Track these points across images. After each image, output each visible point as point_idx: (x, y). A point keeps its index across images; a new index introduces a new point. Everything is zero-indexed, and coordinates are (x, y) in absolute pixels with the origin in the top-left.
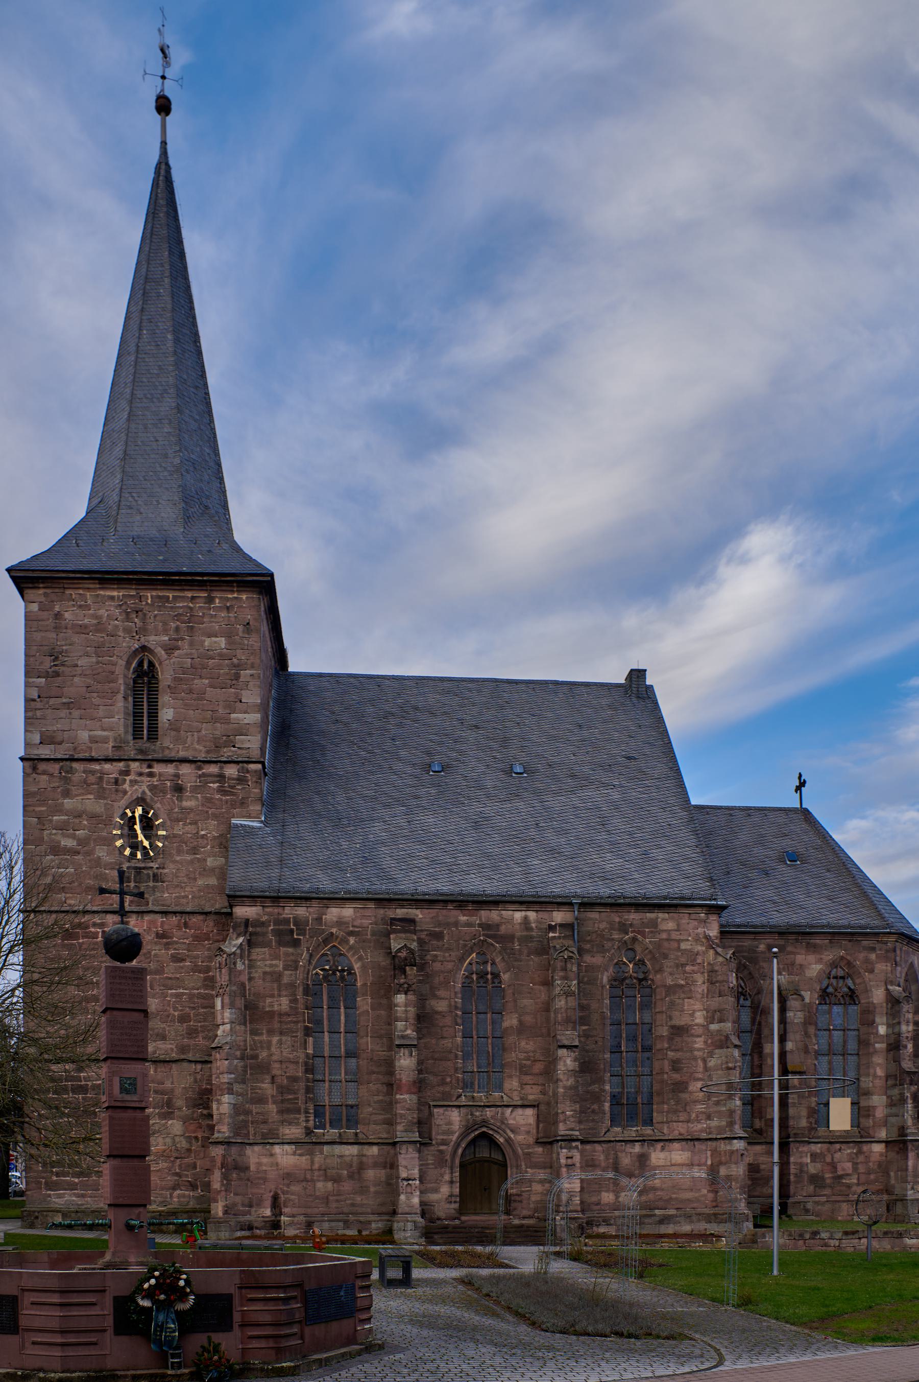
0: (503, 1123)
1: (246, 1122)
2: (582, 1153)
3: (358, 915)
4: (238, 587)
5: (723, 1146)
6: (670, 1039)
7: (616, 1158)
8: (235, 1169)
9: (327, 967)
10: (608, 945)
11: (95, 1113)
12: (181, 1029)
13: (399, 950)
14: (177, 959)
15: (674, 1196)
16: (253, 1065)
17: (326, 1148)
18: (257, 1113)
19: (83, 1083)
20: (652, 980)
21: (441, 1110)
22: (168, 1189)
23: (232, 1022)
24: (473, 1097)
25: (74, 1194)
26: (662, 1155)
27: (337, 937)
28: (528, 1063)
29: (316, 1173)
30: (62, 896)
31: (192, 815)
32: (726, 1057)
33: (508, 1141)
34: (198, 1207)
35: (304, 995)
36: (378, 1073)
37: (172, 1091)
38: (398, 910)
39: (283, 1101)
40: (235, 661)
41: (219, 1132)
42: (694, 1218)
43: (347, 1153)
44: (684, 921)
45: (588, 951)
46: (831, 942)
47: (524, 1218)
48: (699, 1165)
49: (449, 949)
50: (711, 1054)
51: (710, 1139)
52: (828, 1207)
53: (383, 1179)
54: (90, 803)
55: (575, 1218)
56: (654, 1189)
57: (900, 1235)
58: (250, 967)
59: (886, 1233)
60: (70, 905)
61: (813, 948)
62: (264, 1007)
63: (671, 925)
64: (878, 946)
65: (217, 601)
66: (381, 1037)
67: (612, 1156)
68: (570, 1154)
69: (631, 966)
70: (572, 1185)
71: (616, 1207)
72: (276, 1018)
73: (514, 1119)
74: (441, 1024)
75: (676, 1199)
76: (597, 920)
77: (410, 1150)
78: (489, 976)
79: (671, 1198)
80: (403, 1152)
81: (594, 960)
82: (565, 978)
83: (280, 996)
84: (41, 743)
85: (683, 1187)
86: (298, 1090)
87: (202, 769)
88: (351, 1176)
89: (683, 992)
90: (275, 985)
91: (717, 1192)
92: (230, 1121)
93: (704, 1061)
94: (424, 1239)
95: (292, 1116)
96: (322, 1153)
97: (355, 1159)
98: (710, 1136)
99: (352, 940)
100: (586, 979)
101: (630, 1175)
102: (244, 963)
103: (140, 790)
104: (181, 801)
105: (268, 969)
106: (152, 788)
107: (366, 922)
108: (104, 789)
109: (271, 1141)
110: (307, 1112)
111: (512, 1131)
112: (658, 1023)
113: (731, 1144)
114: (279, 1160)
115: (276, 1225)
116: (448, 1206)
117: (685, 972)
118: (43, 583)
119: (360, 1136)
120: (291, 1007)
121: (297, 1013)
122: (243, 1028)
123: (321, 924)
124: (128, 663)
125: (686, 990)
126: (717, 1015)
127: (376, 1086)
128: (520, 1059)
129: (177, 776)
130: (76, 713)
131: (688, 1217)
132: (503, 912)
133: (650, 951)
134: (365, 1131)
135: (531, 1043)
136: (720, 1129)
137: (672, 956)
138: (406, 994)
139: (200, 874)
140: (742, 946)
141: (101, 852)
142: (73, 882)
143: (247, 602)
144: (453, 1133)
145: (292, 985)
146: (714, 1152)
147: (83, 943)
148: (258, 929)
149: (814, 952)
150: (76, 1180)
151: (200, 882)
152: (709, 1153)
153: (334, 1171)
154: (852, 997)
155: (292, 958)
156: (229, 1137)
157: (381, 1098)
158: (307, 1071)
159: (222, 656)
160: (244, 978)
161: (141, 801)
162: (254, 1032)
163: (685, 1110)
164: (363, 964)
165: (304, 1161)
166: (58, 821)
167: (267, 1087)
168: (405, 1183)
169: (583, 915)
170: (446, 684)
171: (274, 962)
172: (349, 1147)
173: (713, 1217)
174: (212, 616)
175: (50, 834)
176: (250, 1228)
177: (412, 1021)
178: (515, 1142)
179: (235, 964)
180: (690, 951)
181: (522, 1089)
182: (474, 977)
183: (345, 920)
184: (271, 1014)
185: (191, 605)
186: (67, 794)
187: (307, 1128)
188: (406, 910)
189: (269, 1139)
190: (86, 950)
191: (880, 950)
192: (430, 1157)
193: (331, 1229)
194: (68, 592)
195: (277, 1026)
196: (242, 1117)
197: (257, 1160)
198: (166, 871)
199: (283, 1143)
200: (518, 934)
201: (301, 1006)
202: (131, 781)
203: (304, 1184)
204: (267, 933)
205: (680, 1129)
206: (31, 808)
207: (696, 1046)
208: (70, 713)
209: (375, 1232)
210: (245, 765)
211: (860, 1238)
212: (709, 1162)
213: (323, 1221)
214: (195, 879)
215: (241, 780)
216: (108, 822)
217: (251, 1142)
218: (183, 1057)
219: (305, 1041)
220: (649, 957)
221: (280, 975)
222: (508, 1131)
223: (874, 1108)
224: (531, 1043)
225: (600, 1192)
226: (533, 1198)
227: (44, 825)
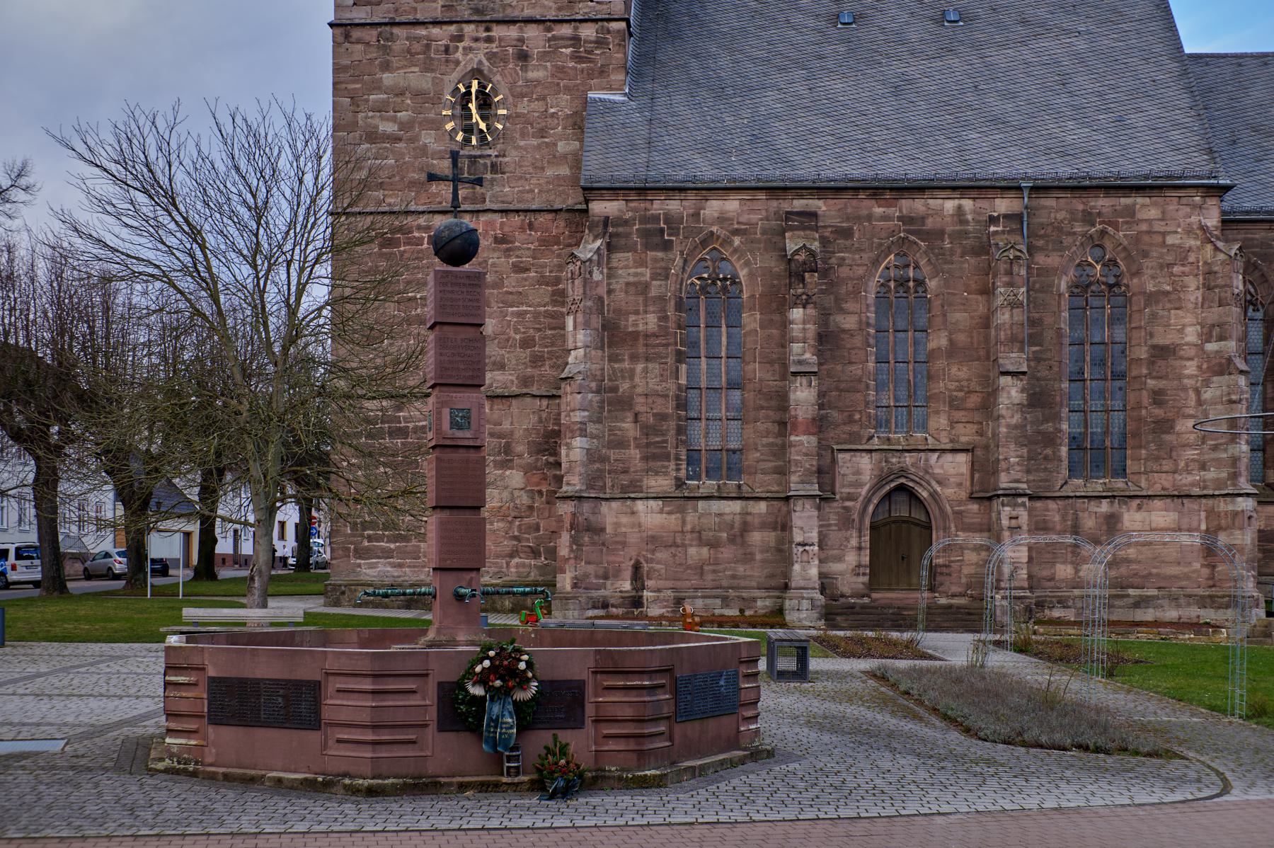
0: (927, 472)
2: (1031, 511)
3: (746, 208)
5: (1223, 506)
7: (1076, 518)
9: (706, 275)
10: (1067, 241)
14: (519, 269)
17: (701, 504)
20: (1127, 286)
21: (847, 456)
22: (503, 557)
24: (889, 439)
25: (390, 563)
27: (718, 237)
28: (961, 394)
29: (689, 536)
31: (539, 89)
32: (1228, 386)
33: (934, 495)
34: (540, 579)
36: (768, 408)
37: (512, 433)
39: (648, 445)
41: (568, 484)
42: (1182, 601)
43: (727, 510)
47: (953, 596)
49: (860, 250)
50: (1207, 383)
51: (1205, 496)
53: (772, 544)
54: (416, 78)
56: (1127, 561)
58: (609, 276)
60: (389, 205)
62: (626, 326)
63: (1153, 213)
66: (771, 362)
68: (1014, 514)
69: (1098, 268)
70: (1016, 554)
72: (641, 341)
73: (942, 467)
74: (849, 346)
76: (1054, 208)
77: (807, 506)
78: (911, 284)
79: (1150, 574)
80: (798, 508)
82: (1010, 284)
83: (646, 312)
88: (732, 540)
90: (641, 299)
91: (1214, 567)
92: (583, 470)
93: (1198, 392)
94: (823, 622)
95: (659, 464)
97: (737, 518)
98: (1205, 492)
99: (737, 241)
102: (602, 273)
103: (476, 60)
105: (631, 279)
106: (491, 56)
107: (754, 217)
109: (632, 495)
111: (939, 483)
112: (1133, 343)
113: (1233, 503)
114: (643, 520)
115: (637, 602)
116: (855, 579)
117: (1172, 274)
119: (745, 488)
121: (667, 334)
122: (600, 353)
123: (698, 221)
126: (1216, 331)
128: (950, 390)
129: (521, 40)
132: (930, 201)
133: (1125, 249)
135: (965, 369)
136: (1219, 483)
141: (428, 138)
145: (661, 299)
146: (1211, 513)
147: (404, 251)
148: (621, 229)
150: (392, 546)
151: (549, 172)
152: (1203, 514)
153: (711, 534)
155: (663, 264)
157: (771, 440)
158: (678, 407)
160: (602, 291)
161: (477, 73)
164: (749, 270)
165: (673, 520)
166: (375, 101)
167: (628, 427)
168: (801, 549)
172: (730, 503)
173: (1208, 600)
175: (367, 117)
176: (605, 606)
177: (812, 342)
178: (943, 497)
179: (591, 273)
181: (952, 428)
182: (892, 284)
184: (635, 336)
186: (386, 67)
187: (677, 479)
188: (805, 202)
189: (630, 492)
193: (706, 608)
195: (641, 350)
198: (506, 159)
201: (671, 325)
202: (464, 48)
203: (673, 550)
204: (631, 233)
206: (343, 86)
209: (762, 612)
212: (1203, 527)
213: (696, 597)
214: (543, 169)
215: (600, 43)
216: (437, 100)
217: (608, 496)
218: (525, 391)
220: (1123, 255)
221: (647, 286)
224: (965, 369)
226: (966, 571)
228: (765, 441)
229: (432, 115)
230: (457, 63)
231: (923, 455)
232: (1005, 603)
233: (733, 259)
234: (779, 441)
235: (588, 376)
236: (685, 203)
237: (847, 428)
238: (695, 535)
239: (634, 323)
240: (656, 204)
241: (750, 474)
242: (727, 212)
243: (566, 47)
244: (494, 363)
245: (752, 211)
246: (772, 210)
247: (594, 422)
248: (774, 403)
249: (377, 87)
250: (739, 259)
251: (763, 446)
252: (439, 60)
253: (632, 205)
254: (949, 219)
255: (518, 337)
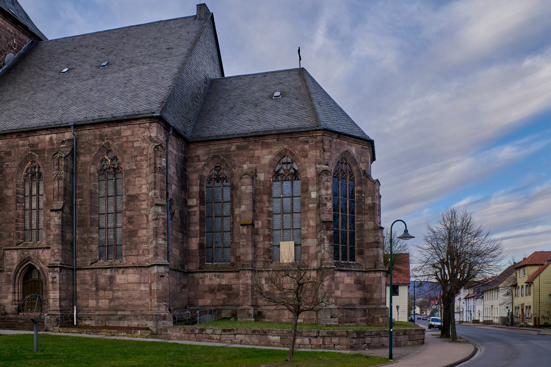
0: (38, 258)
6: (127, 203)
10: (93, 149)
15: (130, 303)
26: (123, 277)
42: (139, 317)
44: (136, 129)
45: (83, 154)
46: (277, 140)
48: (144, 283)
49: (14, 161)
52: (275, 312)
55: (54, 315)
56: (118, 298)
57: (265, 333)
59: (254, 332)
61: (267, 146)
63: (129, 132)
64: (310, 140)
67: (94, 278)
68: (54, 275)
71: (97, 309)
73: (44, 256)
75: (131, 305)
76: (88, 134)
79: (128, 304)
81: (86, 159)
85: (135, 297)
89: (135, 174)
100: (81, 171)
101: (105, 289)
111: (42, 263)
116: (12, 306)
125: (136, 172)
131: (136, 316)
132: (40, 136)
137: (129, 152)
140: (222, 148)
144: (14, 265)
149: (267, 148)
154: (295, 175)
163: (136, 248)
169: (80, 133)
170: (105, 33)
180: (140, 147)
191: (312, 142)
192: (3, 279)
200: (47, 148)
205: (133, 260)
207: (143, 207)
211: (235, 334)
222: (41, 263)
223: (308, 247)
225: (88, 299)
231: (36, 250)
232: (48, 317)
237: (9, 239)
254: (47, 144)
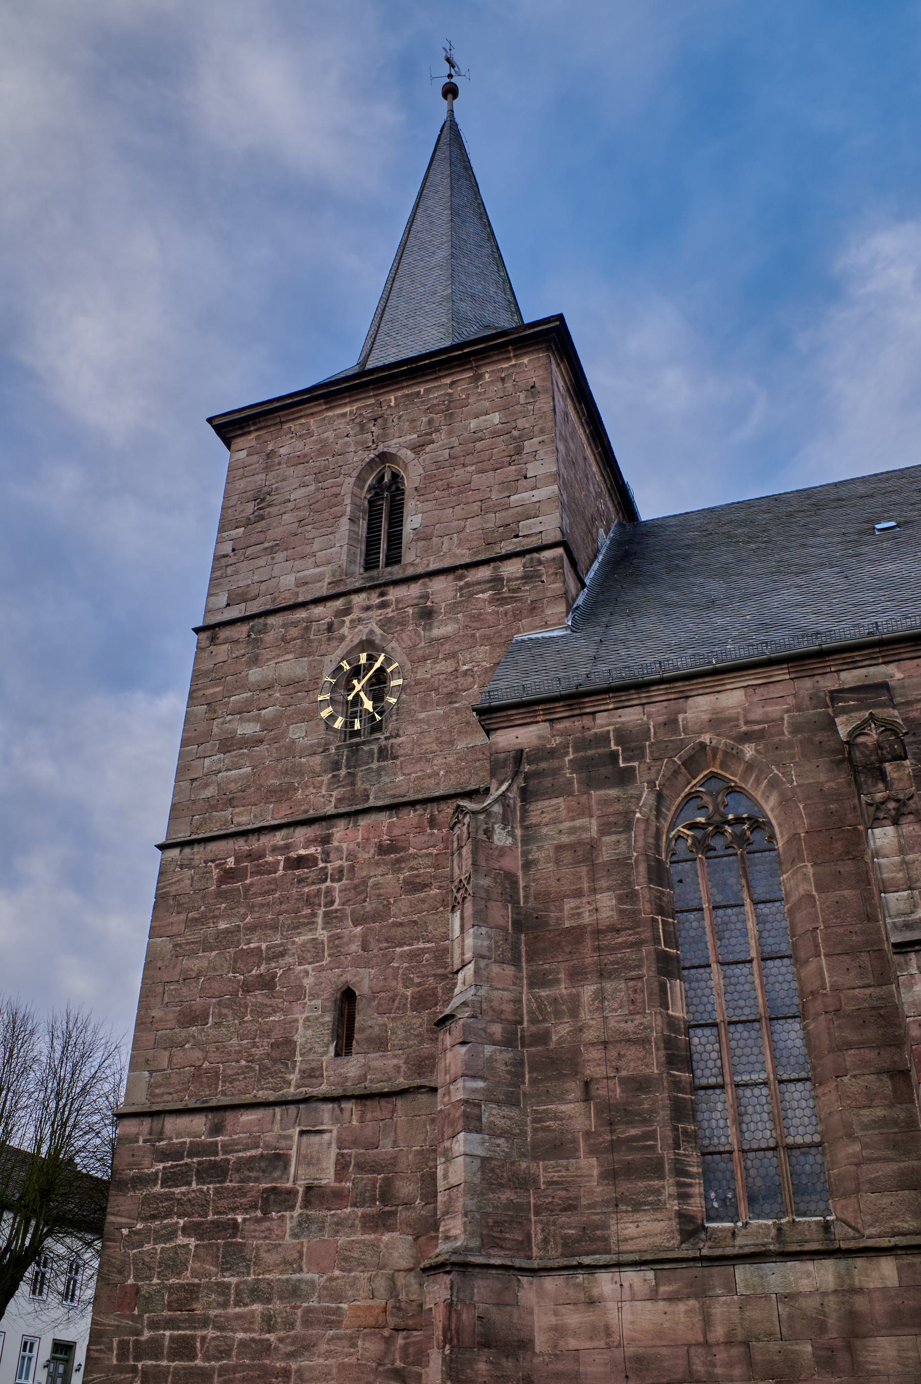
1: (522, 1208)
3: (756, 699)
4: (515, 350)
8: (486, 1345)
11: (235, 1225)
12: (417, 1022)
13: (859, 731)
14: (413, 886)
16: (534, 1059)
17: (742, 1272)
18: (550, 1183)
19: (221, 1157)
23: (478, 956)
27: (715, 750)
29: (721, 1355)
30: (228, 813)
31: (447, 647)
35: (650, 881)
36: (861, 1045)
37: (395, 1159)
38: (843, 675)
39: (614, 1146)
40: (515, 433)
41: (447, 1238)
43: (805, 1285)
54: (292, 667)
58: (526, 841)
60: (239, 825)
62: (559, 920)
65: (487, 376)
66: (853, 952)
72: (589, 942)
83: (594, 891)
84: (228, 605)
86: (652, 1111)
87: (465, 577)
90: (584, 870)
92: (472, 1204)
95: (641, 1184)
96: (731, 1289)
97: (832, 1302)
102: (512, 834)
103: (366, 631)
104: (430, 629)
105: (565, 839)
106: (385, 624)
107: (774, 710)
108: (311, 641)
109: (587, 1260)
110: (680, 1171)
114: (613, 1318)
118: (254, 424)
119: (839, 1230)
120: (621, 912)
121: (637, 924)
122: (509, 970)
123: (676, 731)
124: (360, 480)
127: (862, 1082)
129: (425, 597)
130: (280, 556)
134: (849, 1216)
138: (896, 823)
139: (460, 732)
141: (297, 733)
142: (249, 787)
143: (532, 367)
145: (622, 864)
147: (252, 884)
148: (543, 765)
151: (460, 745)
153: (774, 1346)
155: (619, 807)
156: (467, 1250)
157: (880, 1112)
158: (671, 1061)
159: (495, 434)
160: (513, 863)
161: (368, 645)
162: (538, 981)
165: (680, 1317)
166: (235, 702)
167: (573, 1113)
171: (578, 823)
172: (809, 1266)
174: (480, 394)
175: (223, 723)
179: (489, 833)
183: (727, 714)
184: (577, 934)
185: (450, 391)
186: (255, 661)
187: (683, 1217)
188: (863, 671)
189: (584, 1255)
190: (255, 895)
194: (286, 426)
195: (589, 958)
196: (506, 1195)
197: (553, 1320)
198: (400, 740)
199: (619, 1265)
201: (645, 907)
204: (561, 768)
206: (200, 693)
208: (273, 558)
210: (536, 555)
214: (452, 742)
215: (527, 577)
216: (314, 683)
217: (535, 1264)
218: (419, 1082)
219: (663, 988)
221: (593, 846)
227: (215, 712)
228: (867, 1115)
229: (305, 705)
230: (342, 638)
233: (748, 786)
234: (899, 1113)
235: (478, 1010)
236: (648, 708)
238: (736, 1351)
239: (571, 913)
240: (601, 719)
241: (845, 1196)
242: (724, 710)
243: (482, 592)
244: (370, 1040)
245: (766, 701)
246: (804, 693)
247: (498, 1102)
248: (870, 1033)
249: (242, 686)
250: (758, 782)
251: (865, 1127)
252: (320, 641)
253: (560, 726)
255: (409, 993)
